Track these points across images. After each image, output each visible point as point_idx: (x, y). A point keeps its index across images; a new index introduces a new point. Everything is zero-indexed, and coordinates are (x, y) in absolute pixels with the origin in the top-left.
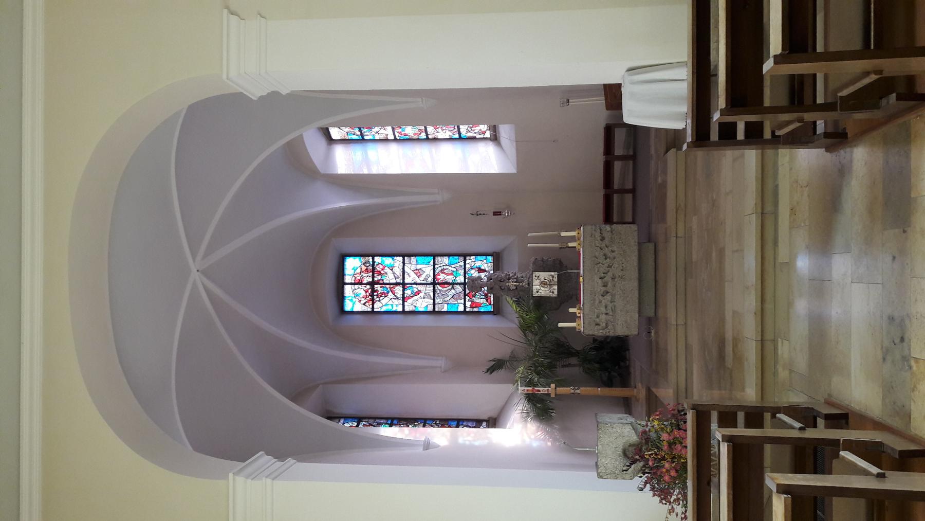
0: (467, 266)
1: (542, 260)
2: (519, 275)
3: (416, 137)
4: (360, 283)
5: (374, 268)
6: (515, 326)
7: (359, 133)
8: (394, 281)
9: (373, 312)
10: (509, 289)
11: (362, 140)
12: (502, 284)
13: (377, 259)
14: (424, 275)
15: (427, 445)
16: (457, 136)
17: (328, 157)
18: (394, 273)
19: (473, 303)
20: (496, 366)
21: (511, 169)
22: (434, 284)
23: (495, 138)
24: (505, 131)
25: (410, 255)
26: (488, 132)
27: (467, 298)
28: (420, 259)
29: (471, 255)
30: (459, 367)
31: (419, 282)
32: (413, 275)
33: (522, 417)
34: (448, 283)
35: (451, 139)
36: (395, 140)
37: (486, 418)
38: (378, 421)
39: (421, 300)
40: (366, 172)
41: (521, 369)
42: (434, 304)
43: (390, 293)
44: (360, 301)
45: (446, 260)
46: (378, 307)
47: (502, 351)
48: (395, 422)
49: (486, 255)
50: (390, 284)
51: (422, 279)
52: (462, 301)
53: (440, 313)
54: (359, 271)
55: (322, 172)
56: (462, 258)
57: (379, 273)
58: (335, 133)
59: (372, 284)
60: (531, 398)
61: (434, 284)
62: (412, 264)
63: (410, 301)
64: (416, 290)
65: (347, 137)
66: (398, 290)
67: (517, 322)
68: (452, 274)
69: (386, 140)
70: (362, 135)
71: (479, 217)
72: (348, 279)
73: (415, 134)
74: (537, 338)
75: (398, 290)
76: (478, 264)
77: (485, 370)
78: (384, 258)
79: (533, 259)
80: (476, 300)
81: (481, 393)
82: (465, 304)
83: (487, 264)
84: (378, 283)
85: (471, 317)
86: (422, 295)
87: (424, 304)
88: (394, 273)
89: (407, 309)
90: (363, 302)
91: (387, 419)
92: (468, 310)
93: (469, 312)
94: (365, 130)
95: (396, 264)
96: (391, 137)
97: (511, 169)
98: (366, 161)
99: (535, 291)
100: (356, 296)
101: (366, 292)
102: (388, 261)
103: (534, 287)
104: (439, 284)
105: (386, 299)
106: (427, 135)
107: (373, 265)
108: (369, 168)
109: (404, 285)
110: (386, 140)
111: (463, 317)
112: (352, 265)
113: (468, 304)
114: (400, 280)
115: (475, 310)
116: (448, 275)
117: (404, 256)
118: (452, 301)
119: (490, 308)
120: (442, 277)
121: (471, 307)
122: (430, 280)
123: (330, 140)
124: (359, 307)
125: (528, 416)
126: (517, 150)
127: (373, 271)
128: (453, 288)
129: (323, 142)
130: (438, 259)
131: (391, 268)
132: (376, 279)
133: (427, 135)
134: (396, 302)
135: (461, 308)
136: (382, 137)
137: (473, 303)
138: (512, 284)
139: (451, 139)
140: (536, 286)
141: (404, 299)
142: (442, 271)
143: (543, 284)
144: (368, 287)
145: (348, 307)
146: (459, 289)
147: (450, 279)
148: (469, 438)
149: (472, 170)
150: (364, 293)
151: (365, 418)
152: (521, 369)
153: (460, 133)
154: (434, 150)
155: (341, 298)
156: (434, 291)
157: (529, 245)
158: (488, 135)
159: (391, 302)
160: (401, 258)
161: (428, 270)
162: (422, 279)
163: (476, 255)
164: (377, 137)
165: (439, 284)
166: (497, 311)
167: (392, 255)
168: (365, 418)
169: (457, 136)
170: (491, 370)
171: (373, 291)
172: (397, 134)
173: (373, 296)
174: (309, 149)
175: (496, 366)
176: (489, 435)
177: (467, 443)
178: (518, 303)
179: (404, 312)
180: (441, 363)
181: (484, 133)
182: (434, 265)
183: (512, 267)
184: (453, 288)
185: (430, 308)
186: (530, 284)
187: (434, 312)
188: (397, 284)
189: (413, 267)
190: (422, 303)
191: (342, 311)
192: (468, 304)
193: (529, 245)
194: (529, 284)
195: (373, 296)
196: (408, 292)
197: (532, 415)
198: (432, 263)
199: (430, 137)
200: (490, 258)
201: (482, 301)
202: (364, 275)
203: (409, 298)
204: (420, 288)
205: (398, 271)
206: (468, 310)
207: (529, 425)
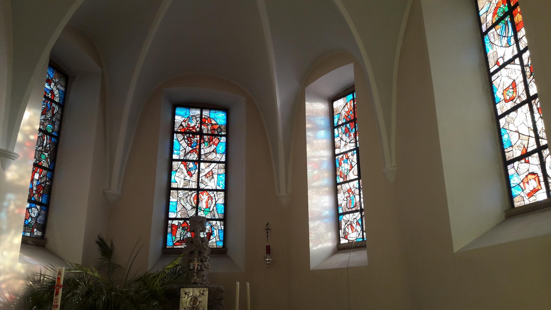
0: (214, 222)
1: (221, 299)
2: (205, 272)
3: (338, 173)
4: (202, 123)
5: (216, 136)
6: (149, 269)
7: (340, 123)
8: (202, 152)
9: (173, 132)
10: (190, 261)
11: (333, 127)
12: (196, 254)
13: (223, 139)
14: (206, 180)
15: (37, 186)
16: (341, 211)
17: (318, 97)
18: (210, 153)
19: (177, 227)
20: (105, 249)
21: (314, 264)
22: (198, 190)
23: (340, 248)
24: (359, 258)
25: (226, 168)
26: (347, 241)
27: (182, 222)
28: (223, 177)
29: (225, 225)
30: (108, 208)
31: (201, 175)
32: (208, 170)
33: (34, 274)
34: (198, 203)
35: (337, 206)
36: (334, 155)
37: (47, 235)
38: (57, 123)
39: (182, 176)
40: (308, 126)
41: (96, 275)
42: (178, 189)
43: (190, 149)
44: (184, 121)
45: (221, 201)
46: (178, 137)
47: (122, 254)
48: (54, 140)
49: (225, 241)
50: (200, 149)
51: (203, 178)
52: (179, 216)
53: (168, 195)
54: (213, 122)
55: (307, 89)
56: (221, 217)
57: (210, 140)
58: (338, 104)
59: (201, 133)
60: (51, 287)
61: (198, 190)
62: (219, 170)
63: (182, 166)
64: (192, 172)
65: (335, 113)
66: (194, 156)
67: (155, 271)
68: (207, 207)
69: (334, 147)
70: (338, 126)
71: (266, 231)
72: (206, 113)
73: (341, 172)
74: (132, 293)
75: (194, 156)
76: (216, 232)
77: (104, 237)
78: (224, 145)
79: (222, 287)
80: (179, 231)
81: (74, 229)
82: (176, 219)
83: (215, 241)
84: (201, 138)
85: (161, 225)
86: (188, 178)
87: (178, 180)
88: (210, 153)
89: (175, 164)
90: (183, 123)
91: (59, 132)
92: (170, 222)
93: (167, 223)
94: (344, 128)
95: (218, 155)
96: (337, 151)
97: (314, 264)
98: (317, 128)
99: (187, 290)
100: (190, 118)
101: (193, 127)
102: (222, 148)
103: (191, 290)
104: (198, 194)
105: (185, 145)
106: (341, 184)
107: (218, 135)
108: (311, 129)
109: (198, 161)
110: (334, 147)
111: (163, 216)
112: (220, 118)
113: (176, 223)
114: (203, 157)
115: (169, 230)
116: (207, 202)
117: (226, 163)
118: (180, 207)
119: (170, 244)
120: (204, 197)
121: (173, 225)
122: (202, 186)
123: (331, 101)
124: (178, 119)
125: (34, 282)
126: (336, 270)
127: (213, 135)
128: (193, 207)
129: (330, 91)
130: (222, 194)
131: (216, 151)
132: (205, 137)
133: (341, 184)
134: (182, 153)
135: (172, 215)
136: (337, 143)
137: (177, 227)
138: (196, 264)
139: (337, 206)
140: (193, 292)
141: (185, 161)
142: (210, 198)
143: (195, 299)
144: (198, 129)
145: (178, 111)
146: (192, 213)
147: (203, 205)
148: (12, 207)
149: (311, 225)
150: (192, 125)
151: (63, 111)
152: (96, 275)
153: (344, 214)
154: (327, 189)
155: (189, 105)
156: (191, 190)
157: (238, 283)
158: (343, 241)
159: (182, 148)
160: (223, 160)
161: (212, 185)
162: (203, 178)
163: (225, 231)
164: (337, 140)
165: (198, 194)
166: (166, 252)
167: (227, 152)
168: (63, 111)
169: (341, 211)
170: (101, 243)
171: (194, 134)
172: (340, 156)
173: (189, 133)
174: (333, 72)
175: (105, 249)
176: (13, 232)
177: (5, 204)
178: (174, 272)
179: (172, 160)
180: (115, 189)
181: (346, 238)
182: (217, 190)
183: (213, 266)
184: (193, 207)
185: (174, 185)
186: (195, 285)
187: (169, 188)
188: (199, 155)
189: (215, 171)
190: (179, 178)
191: (175, 106)
192: (176, 223)
193: (238, 283)
194: (195, 283)
195: (188, 132)
196: (191, 165)
197: (37, 286)
198: (218, 188)
199: (339, 187)
200: (221, 244)
201: (178, 236)
202: (209, 127)
203: (186, 166)
204: (195, 177)
205: (212, 157)
206: (170, 222)
207: (22, 282)
